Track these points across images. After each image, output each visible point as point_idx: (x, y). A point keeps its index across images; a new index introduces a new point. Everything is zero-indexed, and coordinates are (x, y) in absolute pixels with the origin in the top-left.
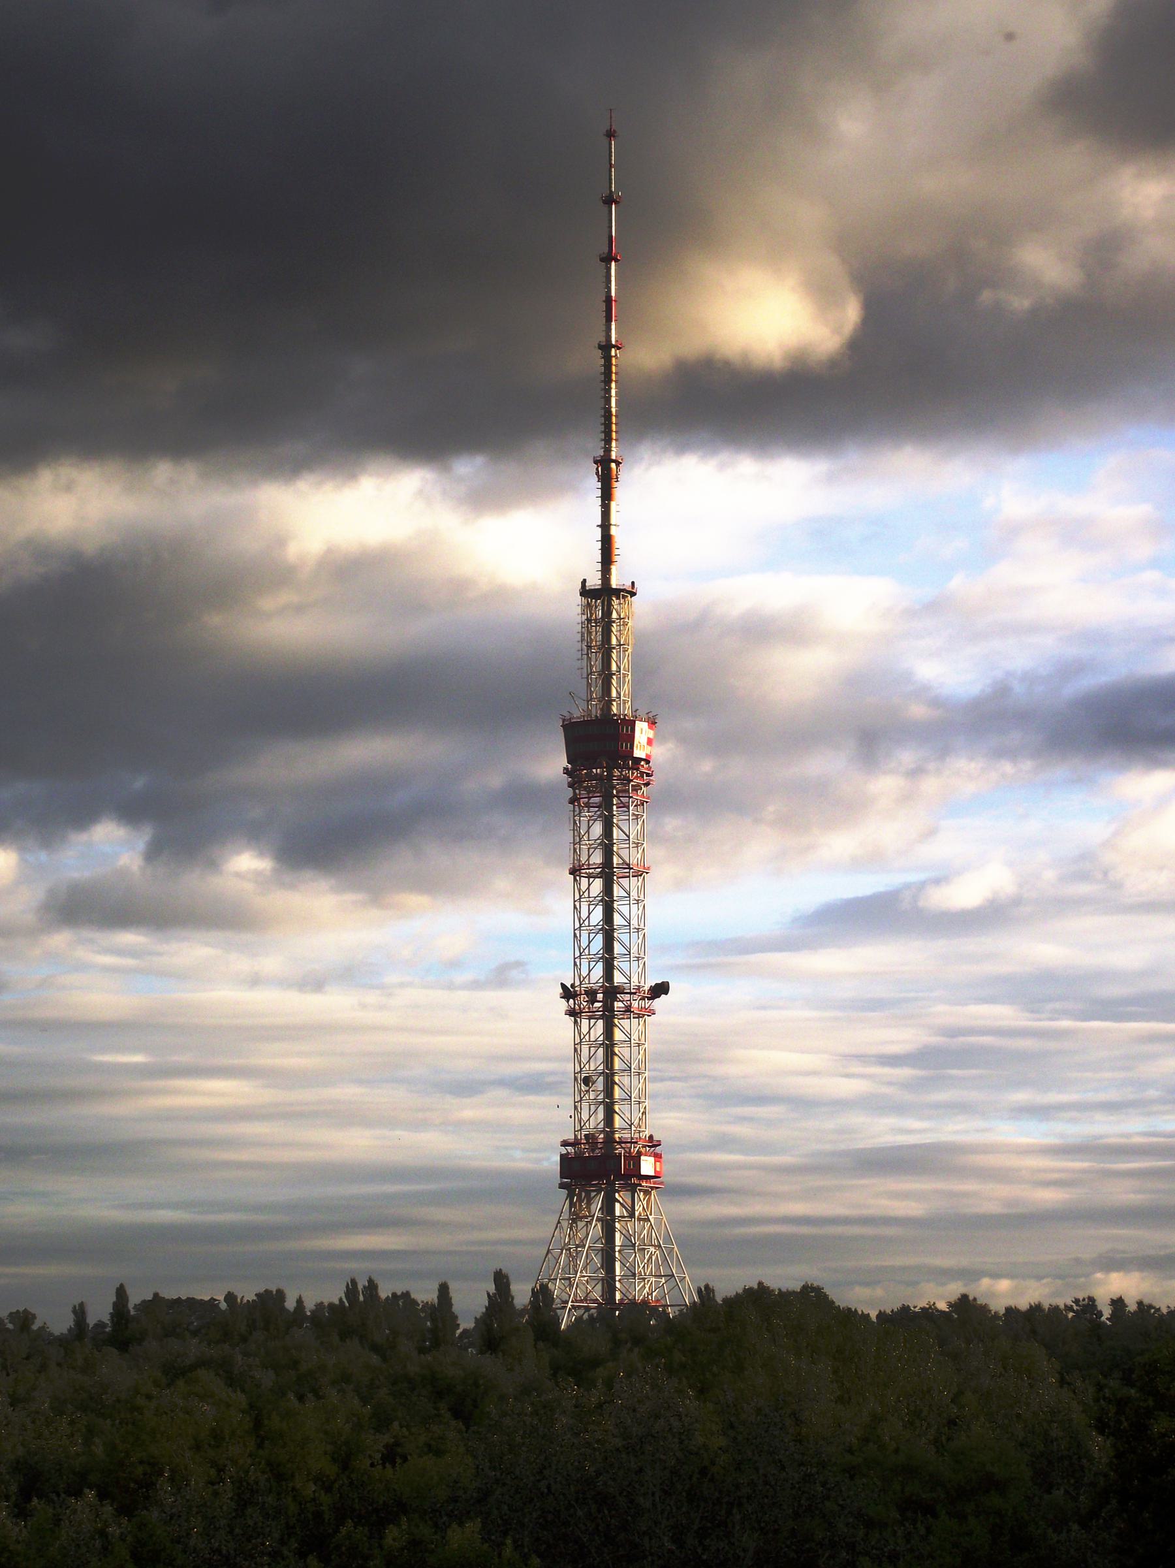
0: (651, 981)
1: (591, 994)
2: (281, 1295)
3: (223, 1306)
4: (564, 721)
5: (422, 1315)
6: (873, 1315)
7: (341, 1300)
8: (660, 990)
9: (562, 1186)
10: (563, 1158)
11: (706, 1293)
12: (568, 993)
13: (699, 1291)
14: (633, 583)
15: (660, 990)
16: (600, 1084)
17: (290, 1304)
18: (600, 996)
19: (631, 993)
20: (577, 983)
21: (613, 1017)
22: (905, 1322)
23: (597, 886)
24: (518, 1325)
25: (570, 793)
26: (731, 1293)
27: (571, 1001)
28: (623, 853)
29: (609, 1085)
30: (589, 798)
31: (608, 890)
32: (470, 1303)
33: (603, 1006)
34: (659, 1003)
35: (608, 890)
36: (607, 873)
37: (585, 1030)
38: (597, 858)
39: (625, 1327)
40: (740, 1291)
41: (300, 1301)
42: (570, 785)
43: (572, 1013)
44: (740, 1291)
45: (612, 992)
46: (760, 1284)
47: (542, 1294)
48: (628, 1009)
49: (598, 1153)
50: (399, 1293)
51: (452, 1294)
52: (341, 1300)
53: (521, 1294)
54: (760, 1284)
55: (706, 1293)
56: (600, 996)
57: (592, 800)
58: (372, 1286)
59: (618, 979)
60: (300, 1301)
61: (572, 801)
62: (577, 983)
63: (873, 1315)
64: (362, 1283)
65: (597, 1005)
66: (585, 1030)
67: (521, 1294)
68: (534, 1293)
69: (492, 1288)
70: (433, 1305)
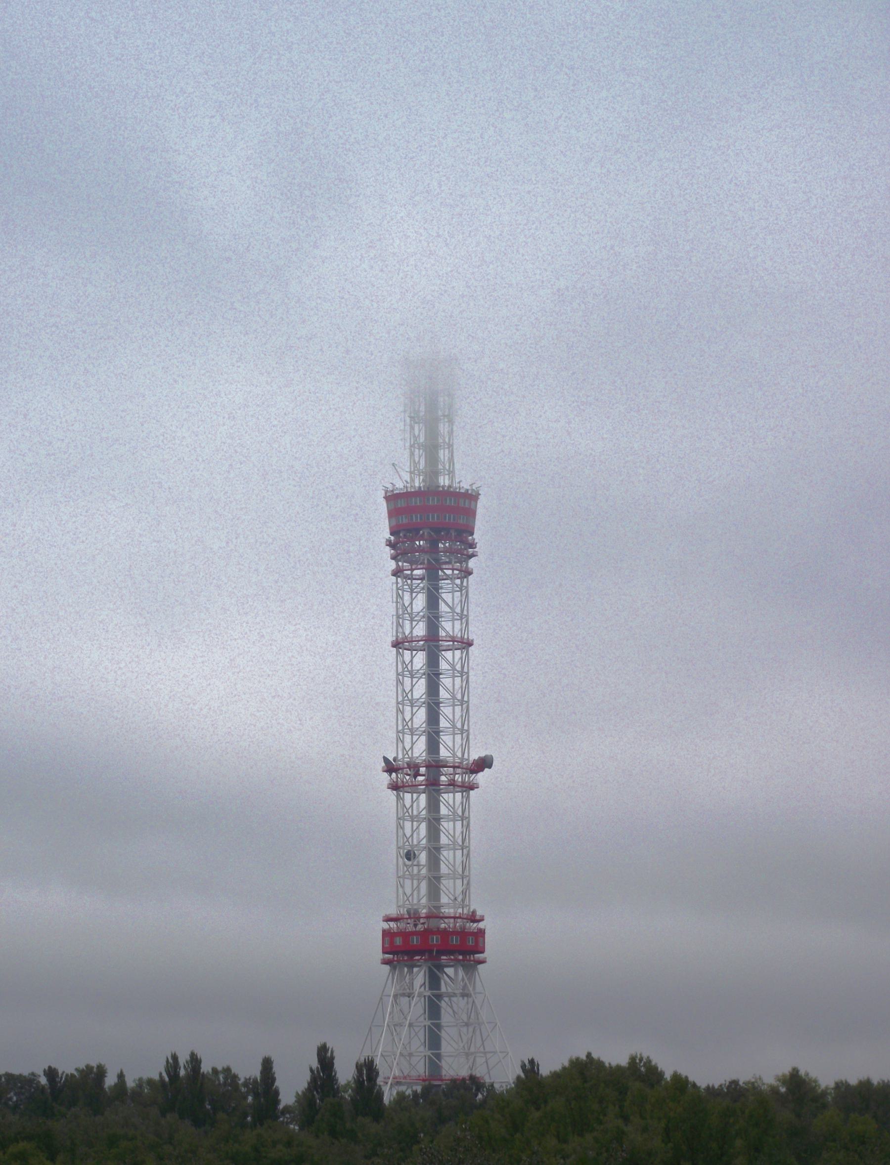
0: (475, 755)
1: (414, 768)
2: (101, 1072)
3: (43, 1081)
4: (386, 492)
5: (243, 1089)
6: (668, 1076)
7: (161, 1074)
8: (484, 764)
9: (385, 962)
10: (386, 933)
11: (531, 1068)
12: (390, 768)
13: (523, 1067)
14: (267, 1064)
15: (484, 764)
16: (423, 857)
17: (110, 1080)
18: (423, 770)
19: (454, 767)
20: (400, 756)
21: (439, 792)
22: (735, 1092)
23: (420, 660)
24: (343, 1105)
25: (393, 565)
26: (557, 1067)
27: (394, 775)
28: (448, 627)
29: (434, 861)
30: (412, 570)
31: (433, 805)
32: (291, 1086)
33: (427, 780)
34: (481, 778)
35: (433, 805)
36: (432, 644)
37: (408, 803)
38: (420, 630)
39: (453, 1101)
40: (567, 1064)
41: (121, 1076)
42: (394, 558)
43: (395, 787)
44: (567, 1064)
45: (435, 766)
46: (589, 1055)
47: (367, 1071)
48: (452, 783)
49: (420, 927)
50: (220, 1068)
51: (276, 1069)
52: (161, 1074)
53: (345, 1073)
54: (589, 1055)
55: (531, 1068)
56: (423, 770)
57: (416, 572)
58: (195, 1061)
59: (444, 753)
60: (121, 1076)
61: (397, 573)
62: (400, 756)
63: (668, 1076)
64: (183, 1059)
65: (420, 778)
66: (408, 803)
67: (345, 1073)
68: (359, 1067)
69: (315, 1064)
70: (255, 1081)
